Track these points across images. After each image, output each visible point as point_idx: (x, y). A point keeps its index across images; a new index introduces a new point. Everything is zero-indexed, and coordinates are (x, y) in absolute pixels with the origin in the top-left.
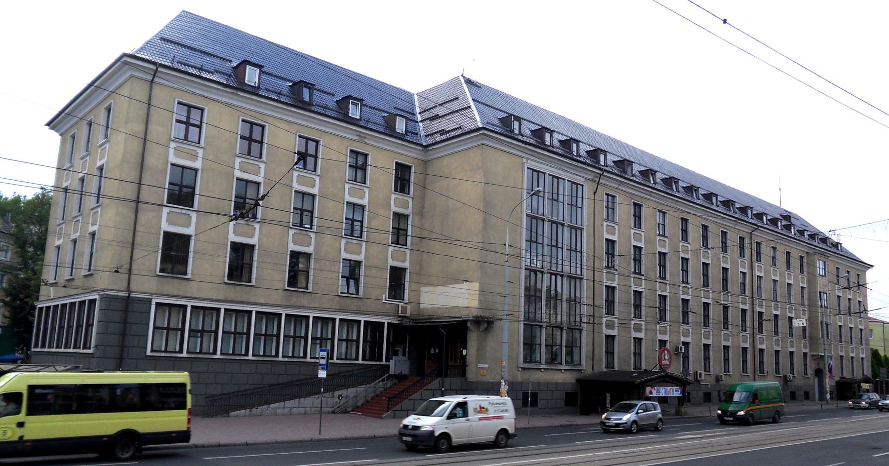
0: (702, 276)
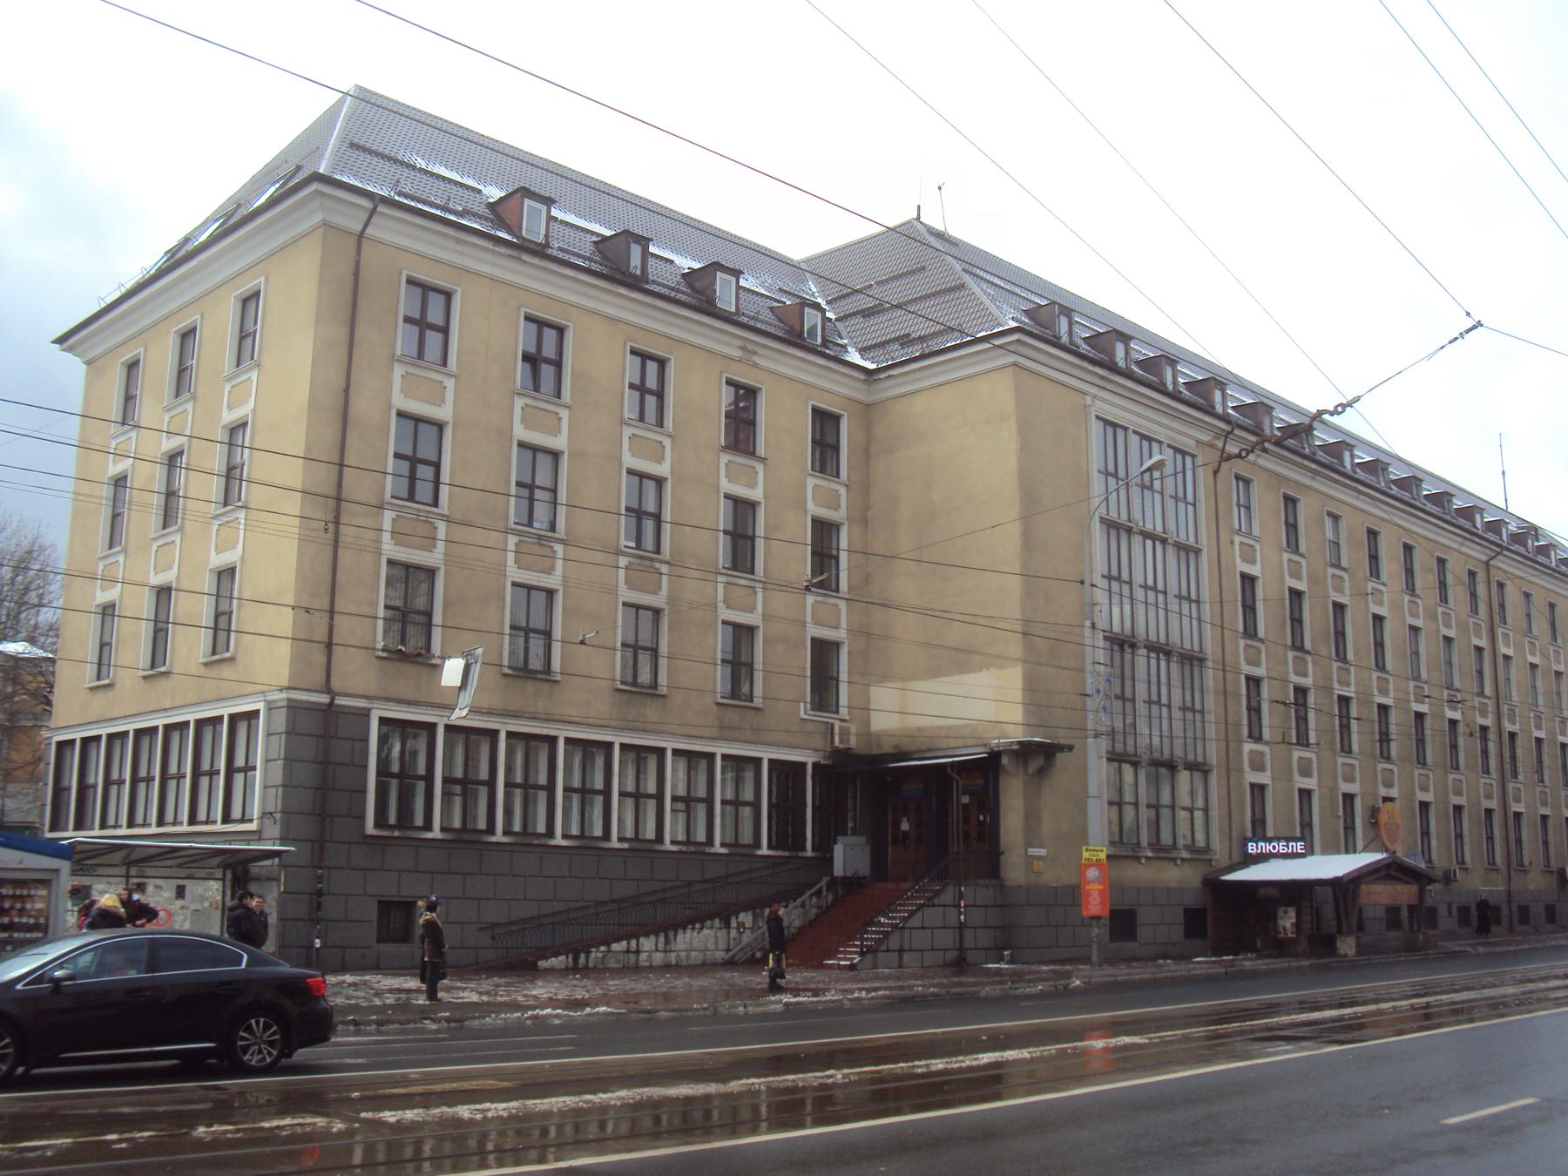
0: (1240, 608)
